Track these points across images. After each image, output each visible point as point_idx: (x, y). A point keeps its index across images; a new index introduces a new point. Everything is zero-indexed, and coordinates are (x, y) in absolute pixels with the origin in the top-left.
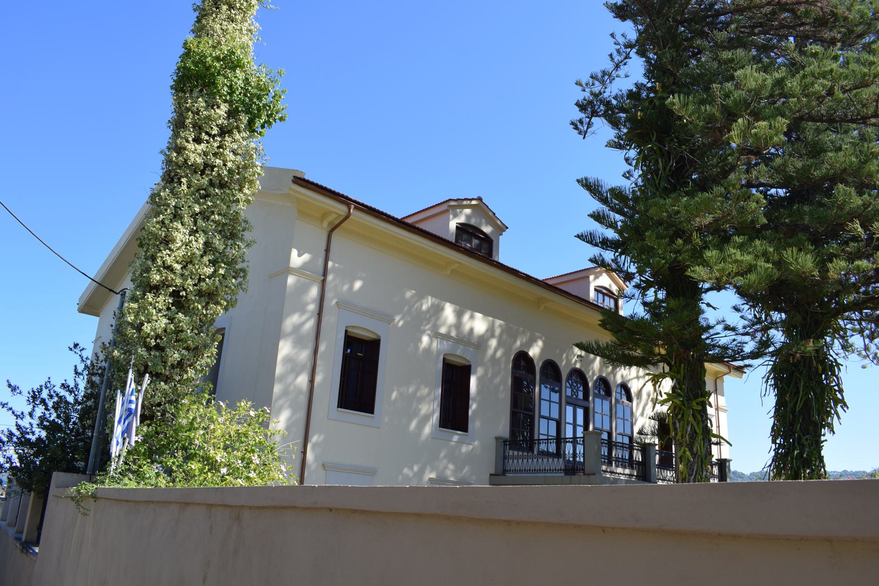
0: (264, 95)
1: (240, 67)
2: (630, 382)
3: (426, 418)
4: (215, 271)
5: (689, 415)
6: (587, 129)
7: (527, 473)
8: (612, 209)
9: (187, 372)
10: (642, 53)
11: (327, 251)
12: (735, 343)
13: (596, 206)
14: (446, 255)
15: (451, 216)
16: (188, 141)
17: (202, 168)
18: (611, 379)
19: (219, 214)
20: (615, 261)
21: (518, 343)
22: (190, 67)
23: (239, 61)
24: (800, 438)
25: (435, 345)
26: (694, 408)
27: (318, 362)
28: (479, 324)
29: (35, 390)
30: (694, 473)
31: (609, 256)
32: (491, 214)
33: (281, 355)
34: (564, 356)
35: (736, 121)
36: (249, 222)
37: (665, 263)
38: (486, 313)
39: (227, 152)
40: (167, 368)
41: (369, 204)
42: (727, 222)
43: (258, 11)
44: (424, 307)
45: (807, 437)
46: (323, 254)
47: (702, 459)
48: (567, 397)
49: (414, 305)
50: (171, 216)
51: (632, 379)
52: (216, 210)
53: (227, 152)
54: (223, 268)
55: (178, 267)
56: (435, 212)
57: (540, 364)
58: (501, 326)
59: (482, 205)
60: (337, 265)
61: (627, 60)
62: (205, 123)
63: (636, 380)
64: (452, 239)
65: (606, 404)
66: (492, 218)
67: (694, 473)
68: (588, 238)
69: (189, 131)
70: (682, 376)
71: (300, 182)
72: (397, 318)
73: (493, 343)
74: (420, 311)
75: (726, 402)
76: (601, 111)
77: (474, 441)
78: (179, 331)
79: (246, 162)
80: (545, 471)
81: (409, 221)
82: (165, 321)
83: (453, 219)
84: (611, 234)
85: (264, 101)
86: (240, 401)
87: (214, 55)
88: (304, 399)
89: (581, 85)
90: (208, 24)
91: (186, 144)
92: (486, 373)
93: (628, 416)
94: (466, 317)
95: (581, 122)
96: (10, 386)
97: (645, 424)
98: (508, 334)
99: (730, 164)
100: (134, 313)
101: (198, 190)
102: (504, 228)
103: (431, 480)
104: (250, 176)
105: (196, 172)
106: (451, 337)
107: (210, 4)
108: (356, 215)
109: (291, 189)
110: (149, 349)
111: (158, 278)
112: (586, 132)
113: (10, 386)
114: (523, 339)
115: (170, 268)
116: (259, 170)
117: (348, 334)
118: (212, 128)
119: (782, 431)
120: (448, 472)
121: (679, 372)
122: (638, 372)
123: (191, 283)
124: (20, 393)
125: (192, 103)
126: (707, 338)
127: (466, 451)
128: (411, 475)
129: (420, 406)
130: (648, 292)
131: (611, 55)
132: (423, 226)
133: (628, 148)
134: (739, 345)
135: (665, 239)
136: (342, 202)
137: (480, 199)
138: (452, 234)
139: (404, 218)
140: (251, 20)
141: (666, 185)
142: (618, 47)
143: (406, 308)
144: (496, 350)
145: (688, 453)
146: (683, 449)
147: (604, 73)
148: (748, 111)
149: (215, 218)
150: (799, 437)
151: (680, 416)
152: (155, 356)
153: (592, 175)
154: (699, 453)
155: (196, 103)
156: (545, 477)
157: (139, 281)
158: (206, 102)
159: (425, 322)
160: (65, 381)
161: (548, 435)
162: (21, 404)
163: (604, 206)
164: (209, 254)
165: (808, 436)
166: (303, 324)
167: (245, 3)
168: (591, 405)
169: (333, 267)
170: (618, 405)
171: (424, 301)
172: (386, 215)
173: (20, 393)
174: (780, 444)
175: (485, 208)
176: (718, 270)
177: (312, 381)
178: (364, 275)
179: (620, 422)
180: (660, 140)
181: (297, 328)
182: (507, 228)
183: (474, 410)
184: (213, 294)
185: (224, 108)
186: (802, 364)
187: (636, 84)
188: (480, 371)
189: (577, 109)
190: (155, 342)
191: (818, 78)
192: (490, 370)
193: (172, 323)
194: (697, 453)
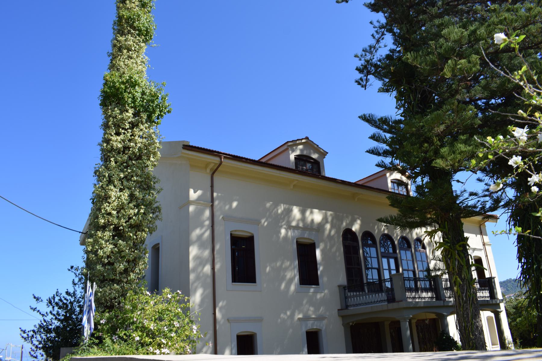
0: (155, 100)
1: (137, 85)
3: (291, 280)
4: (139, 211)
5: (455, 254)
6: (366, 83)
7: (361, 305)
8: (385, 131)
9: (130, 275)
10: (390, 31)
11: (212, 186)
12: (480, 203)
13: (373, 130)
15: (290, 152)
16: (112, 135)
17: (122, 149)
18: (409, 237)
19: (137, 176)
20: (391, 163)
21: (344, 224)
22: (107, 91)
23: (136, 81)
24: (536, 257)
25: (289, 233)
26: (458, 249)
27: (216, 256)
28: (317, 216)
29: (51, 298)
30: (465, 291)
31: (388, 160)
32: (316, 146)
33: (191, 257)
34: (376, 227)
35: (447, 62)
36: (157, 177)
37: (418, 160)
38: (320, 209)
39: (136, 138)
40: (117, 275)
41: (233, 154)
42: (455, 127)
43: (146, 49)
44: (280, 211)
46: (210, 189)
47: (469, 282)
48: (382, 253)
50: (107, 183)
52: (134, 174)
53: (136, 138)
54: (143, 208)
55: (114, 212)
56: (276, 154)
57: (361, 235)
58: (331, 215)
59: (309, 141)
60: (219, 194)
61: (383, 36)
62: (121, 123)
64: (294, 168)
65: (409, 253)
66: (317, 149)
67: (465, 291)
68: (373, 152)
69: (112, 129)
70: (447, 230)
71: (188, 148)
72: (263, 221)
73: (328, 226)
75: (489, 239)
76: (372, 70)
77: (324, 290)
78: (120, 251)
79: (149, 142)
80: (371, 303)
81: (264, 160)
82: (111, 246)
83: (292, 153)
84: (385, 147)
85: (156, 103)
86: (164, 289)
87: (120, 81)
88: (210, 280)
89: (358, 57)
90: (116, 62)
91: (111, 137)
92: (326, 246)
93: (424, 258)
94: (308, 213)
95: (361, 79)
96: (35, 297)
98: (336, 221)
99: (454, 89)
100: (91, 245)
101: (122, 164)
102: (326, 153)
103: (299, 319)
104: (153, 149)
105: (119, 153)
106: (300, 227)
107: (116, 51)
110: (104, 265)
111: (103, 221)
112: (366, 86)
113: (35, 297)
114: (347, 221)
115: (110, 214)
116: (158, 145)
117: (233, 235)
118: (125, 125)
119: (524, 254)
120: (310, 313)
121: (445, 228)
123: (123, 221)
124: (42, 301)
125: (111, 112)
126: (460, 203)
127: (320, 298)
128: (286, 317)
129: (286, 274)
130: (417, 180)
131: (373, 35)
132: (272, 162)
133: (391, 90)
134: (483, 203)
135: (416, 145)
136: (216, 155)
137: (307, 138)
138: (293, 163)
139: (260, 159)
140: (143, 55)
141: (417, 110)
142: (376, 29)
143: (268, 213)
144: (330, 231)
145: (458, 279)
146: (455, 276)
147: (371, 47)
148: (455, 54)
149: (134, 179)
150: (536, 256)
151: (449, 256)
152: (108, 269)
154: (466, 278)
155: (114, 111)
156: (371, 307)
157: (93, 225)
158: (120, 110)
159: (281, 221)
160: (67, 290)
161: (373, 279)
162: (44, 307)
163: (379, 130)
164: (134, 202)
166: (203, 234)
167: (137, 46)
168: (399, 256)
170: (416, 253)
171: (279, 207)
172: (245, 158)
173: (42, 301)
174: (524, 263)
175: (312, 143)
176: (450, 160)
177: (213, 268)
179: (420, 263)
180: (409, 83)
181: (200, 237)
182: (327, 153)
183: (322, 271)
184: (139, 225)
185: (131, 111)
186: (530, 208)
187: (390, 50)
188: (322, 245)
189: (357, 72)
190: (107, 260)
191: (497, 25)
192: (328, 244)
193: (116, 247)
194: (465, 278)
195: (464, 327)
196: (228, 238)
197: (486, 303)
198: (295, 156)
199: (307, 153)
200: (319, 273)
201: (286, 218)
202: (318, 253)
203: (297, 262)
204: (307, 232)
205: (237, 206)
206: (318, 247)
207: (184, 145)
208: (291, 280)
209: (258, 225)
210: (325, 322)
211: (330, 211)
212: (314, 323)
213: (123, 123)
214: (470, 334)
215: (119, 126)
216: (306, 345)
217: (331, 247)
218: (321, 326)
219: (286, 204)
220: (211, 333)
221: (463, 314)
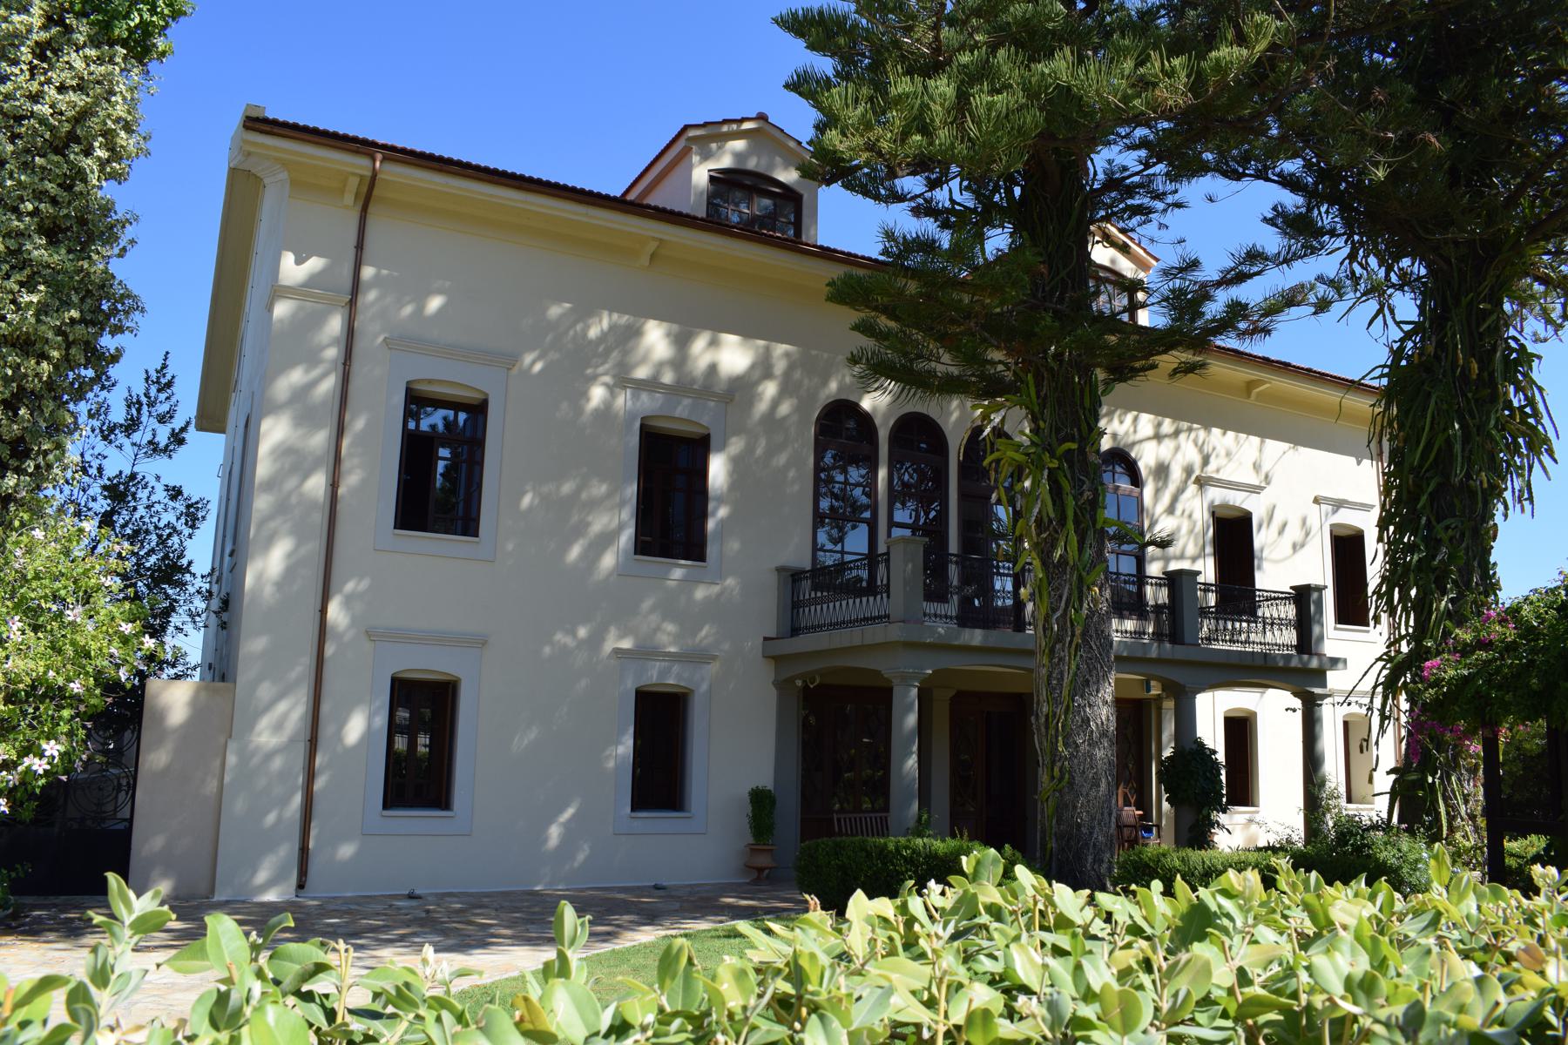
2: (1136, 448)
3: (607, 539)
11: (360, 246)
21: (833, 386)
32: (792, 144)
33: (264, 448)
38: (747, 332)
44: (593, 333)
45: (1447, 522)
46: (351, 253)
51: (1141, 441)
58: (787, 355)
60: (385, 272)
63: (1154, 443)
73: (770, 389)
74: (583, 344)
83: (701, 163)
88: (319, 519)
92: (750, 449)
94: (699, 344)
97: (1179, 529)
103: (618, 652)
108: (395, 174)
114: (844, 376)
120: (663, 638)
122: (1159, 425)
129: (590, 518)
137: (762, 117)
138: (702, 193)
143: (549, 338)
144: (775, 403)
165: (1452, 520)
166: (313, 384)
169: (377, 276)
172: (459, 163)
177: (334, 485)
178: (448, 284)
181: (301, 394)
188: (736, 445)
192: (762, 443)
195: (1047, 716)
197: (1260, 662)
198: (712, 173)
200: (711, 524)
201: (615, 355)
202: (718, 469)
203: (632, 490)
204: (687, 401)
206: (722, 448)
208: (607, 539)
210: (713, 668)
213: (12, 45)
214: (1057, 741)
216: (631, 730)
217: (771, 452)
218: (700, 681)
220: (303, 666)
221: (1050, 676)
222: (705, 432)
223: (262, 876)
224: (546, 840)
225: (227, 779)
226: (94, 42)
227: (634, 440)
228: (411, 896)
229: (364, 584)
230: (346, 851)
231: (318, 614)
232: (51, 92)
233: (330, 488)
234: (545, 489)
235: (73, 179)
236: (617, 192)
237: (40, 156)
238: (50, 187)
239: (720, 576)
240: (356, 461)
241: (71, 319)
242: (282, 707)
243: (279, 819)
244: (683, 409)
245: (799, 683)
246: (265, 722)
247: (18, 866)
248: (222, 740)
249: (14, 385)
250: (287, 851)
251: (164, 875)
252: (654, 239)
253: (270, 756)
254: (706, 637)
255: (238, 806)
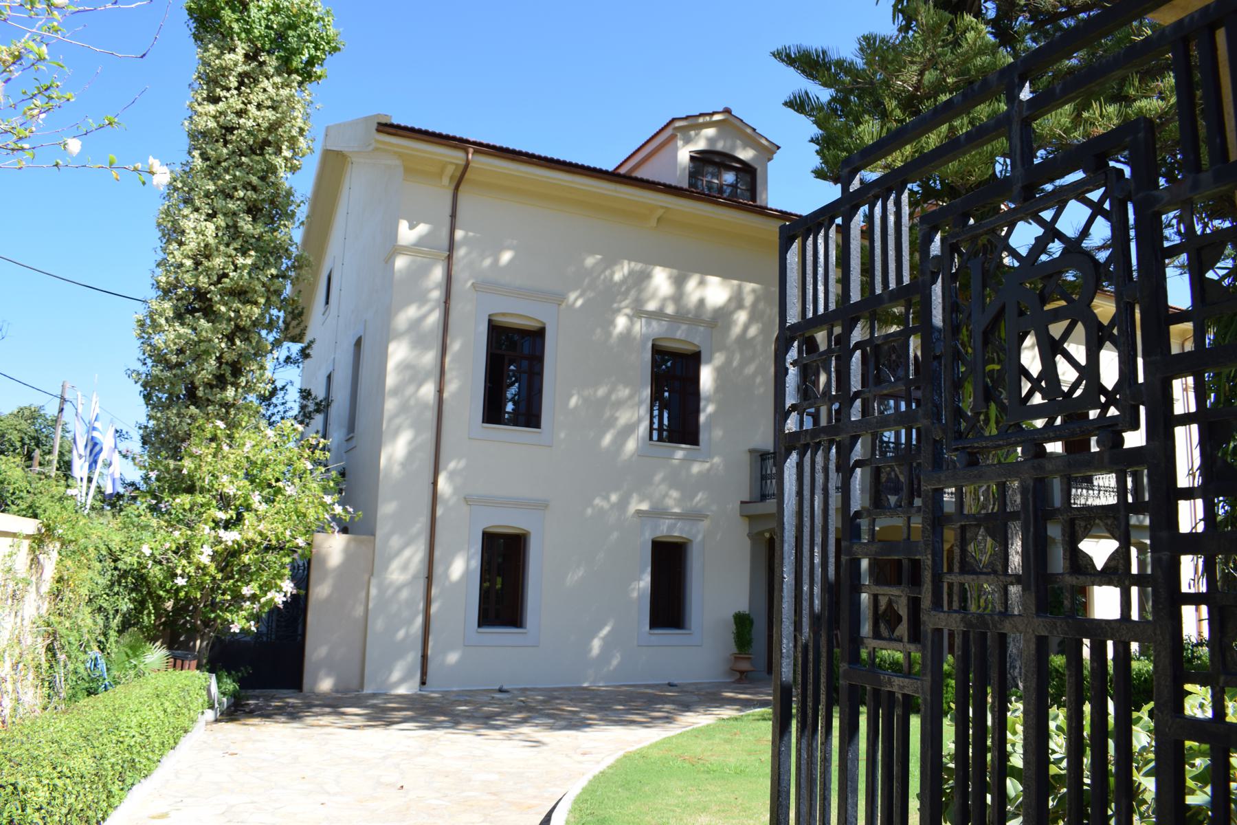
3: (629, 429)
11: (453, 215)
14: (627, 197)
32: (749, 131)
33: (391, 364)
38: (725, 274)
44: (618, 277)
46: (447, 220)
49: (599, 275)
58: (754, 291)
59: (731, 119)
60: (471, 234)
66: (751, 137)
73: (742, 317)
77: (712, 458)
83: (684, 146)
88: (430, 416)
92: (728, 362)
94: (692, 284)
102: (776, 148)
103: (639, 512)
109: (377, 141)
120: (669, 502)
129: (617, 414)
137: (727, 111)
138: (685, 169)
143: (586, 281)
149: (239, 195)
153: (813, 41)
166: (424, 317)
169: (465, 237)
171: (617, 268)
172: (527, 154)
175: (739, 123)
177: (440, 391)
178: (515, 242)
181: (416, 324)
182: (779, 148)
188: (719, 358)
192: (737, 357)
196: (484, 328)
198: (692, 154)
199: (724, 146)
200: (702, 418)
201: (633, 293)
202: (707, 377)
204: (684, 327)
205: (512, 261)
206: (709, 361)
207: (380, 124)
208: (629, 429)
209: (559, 305)
210: (705, 524)
211: (750, 282)
212: (675, 525)
213: (223, 76)
215: (217, 83)
216: (649, 569)
217: (744, 363)
218: (696, 534)
219: (637, 260)
220: (422, 522)
222: (697, 349)
223: (396, 675)
224: (591, 650)
225: (371, 605)
226: (278, 71)
227: (648, 356)
228: (501, 691)
229: (462, 464)
230: (453, 658)
231: (431, 486)
232: (252, 109)
233: (437, 393)
234: (586, 393)
235: (267, 172)
236: (611, 168)
237: (245, 156)
238: (254, 180)
239: (710, 456)
240: (454, 373)
241: (272, 275)
242: (407, 553)
243: (407, 636)
244: (681, 333)
245: (767, 535)
246: (395, 565)
247: (242, 668)
248: (366, 577)
249: (232, 323)
250: (413, 657)
251: (328, 675)
252: (662, 207)
253: (399, 589)
254: (700, 500)
255: (378, 624)
